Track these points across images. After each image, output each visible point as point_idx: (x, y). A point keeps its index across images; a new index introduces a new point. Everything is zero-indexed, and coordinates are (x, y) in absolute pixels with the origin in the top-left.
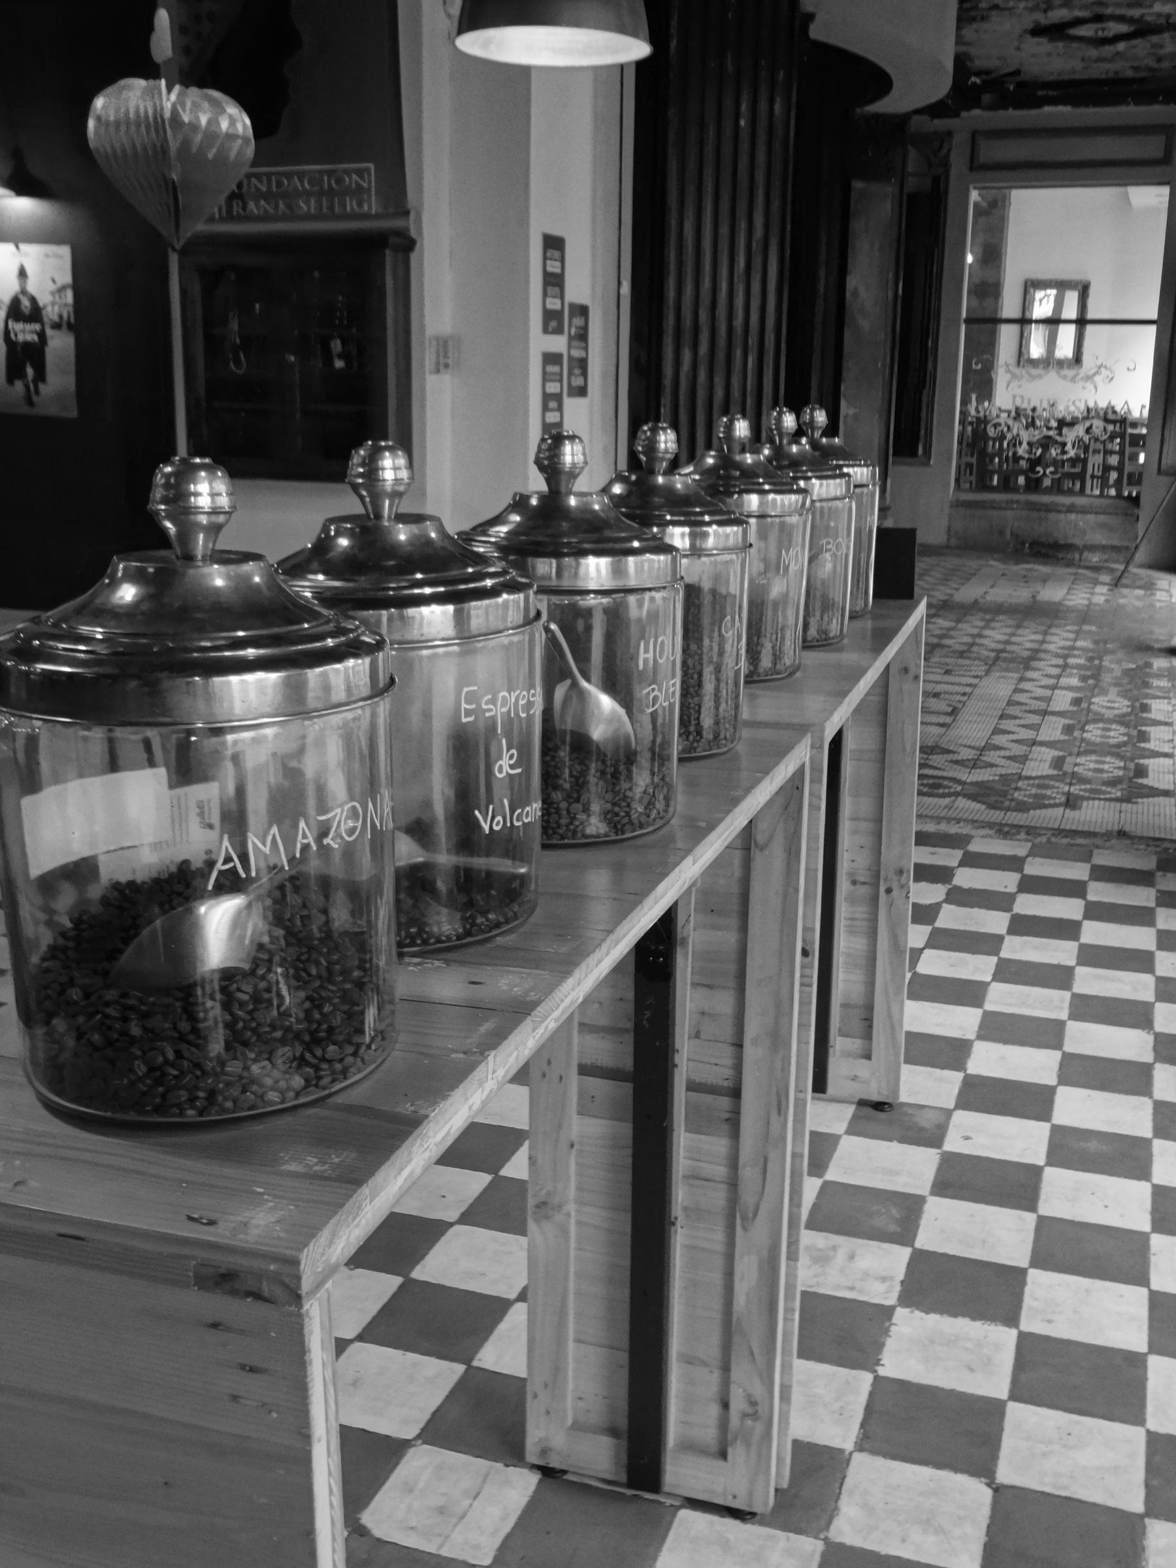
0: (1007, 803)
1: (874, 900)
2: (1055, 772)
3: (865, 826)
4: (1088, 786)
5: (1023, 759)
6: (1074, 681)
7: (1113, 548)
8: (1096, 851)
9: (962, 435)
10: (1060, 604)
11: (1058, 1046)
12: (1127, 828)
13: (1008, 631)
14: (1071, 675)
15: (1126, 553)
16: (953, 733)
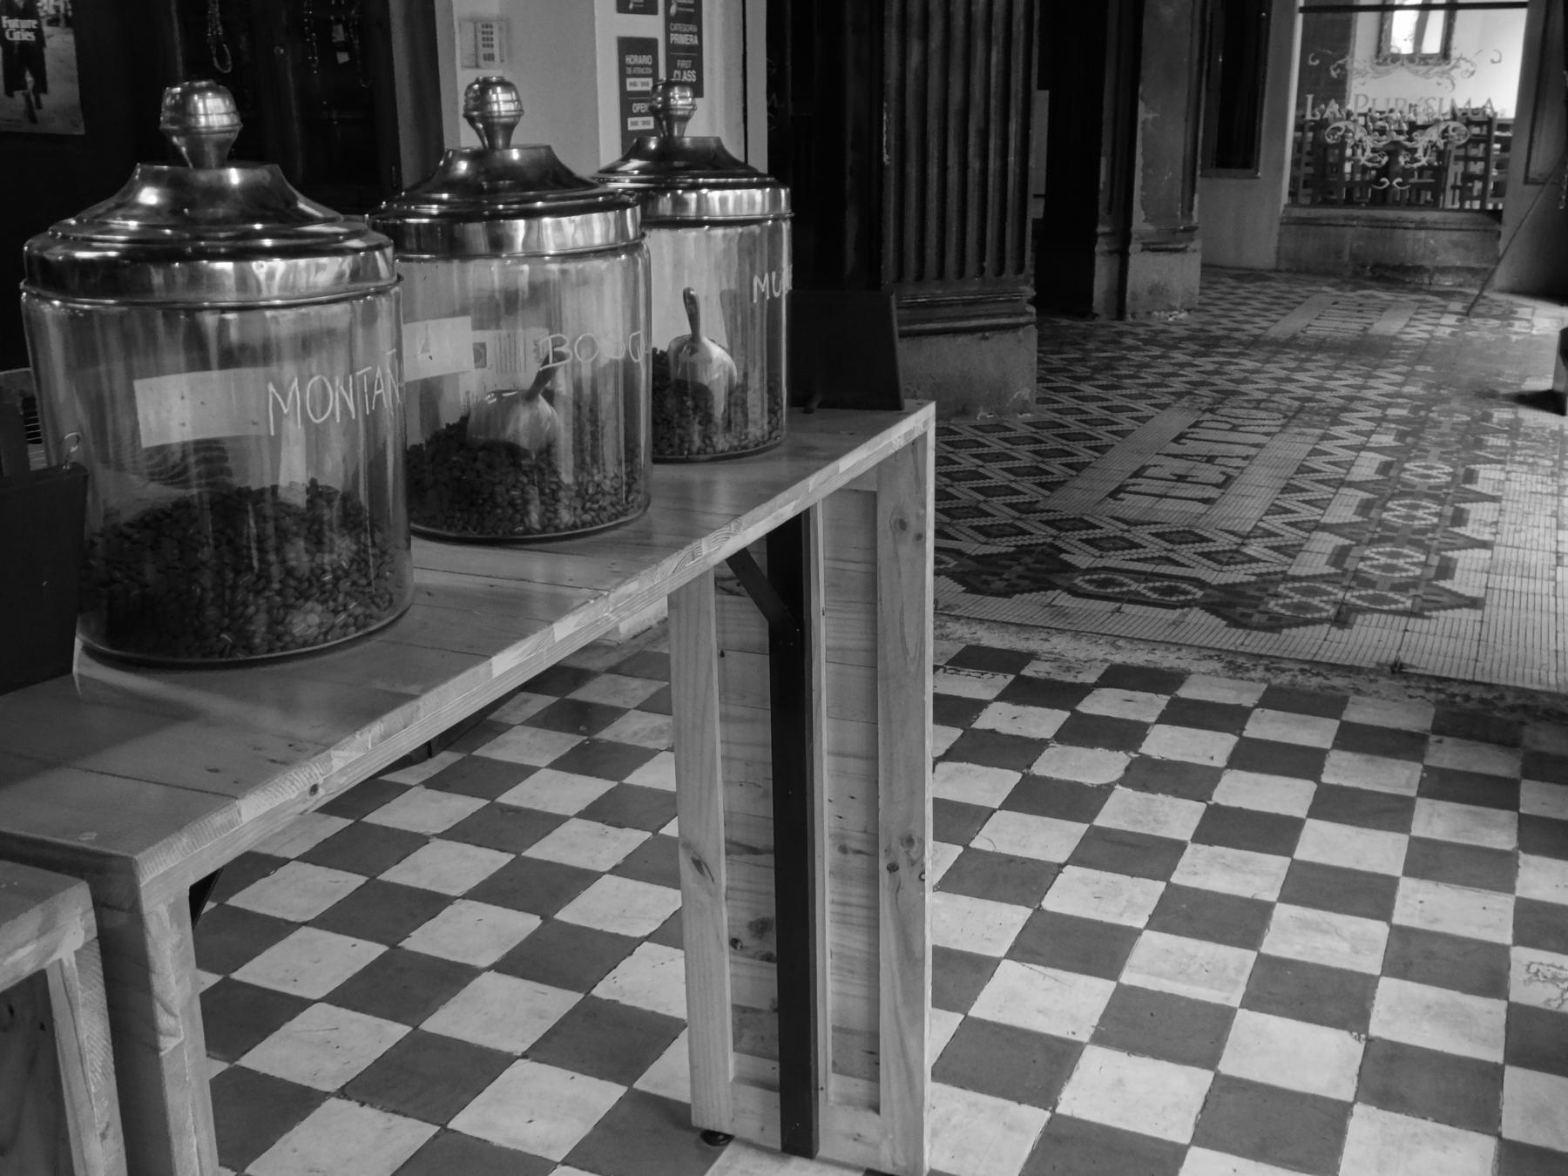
0: (1256, 618)
1: (873, 879)
2: (1333, 570)
3: (856, 766)
4: (1371, 592)
5: (1290, 551)
6: (1388, 440)
7: (1470, 270)
8: (1353, 698)
9: (1298, 145)
10: (1394, 338)
11: (1209, 1060)
12: (1407, 659)
13: (1324, 373)
14: (1387, 432)
15: (1484, 276)
16: (1216, 512)
